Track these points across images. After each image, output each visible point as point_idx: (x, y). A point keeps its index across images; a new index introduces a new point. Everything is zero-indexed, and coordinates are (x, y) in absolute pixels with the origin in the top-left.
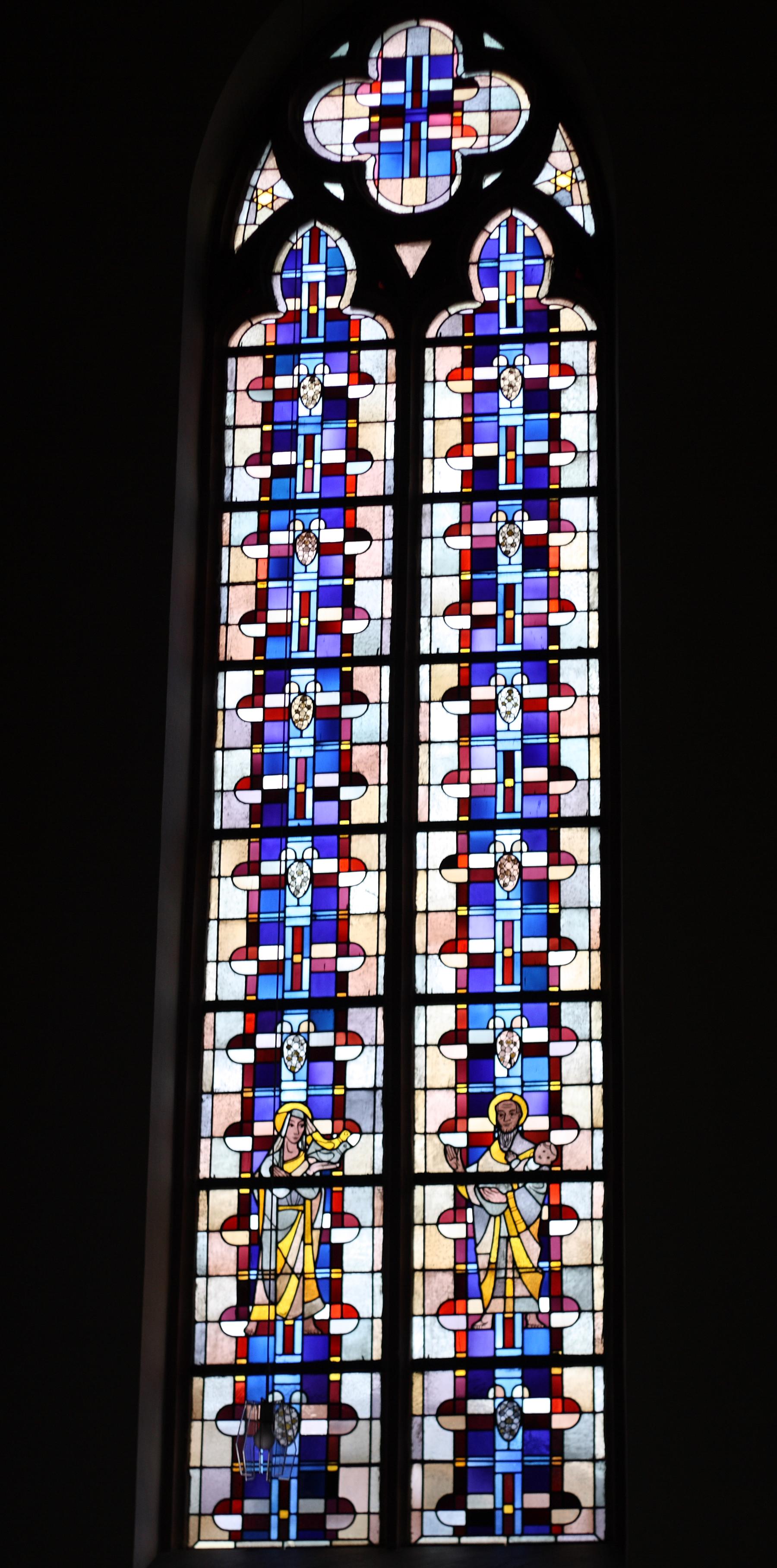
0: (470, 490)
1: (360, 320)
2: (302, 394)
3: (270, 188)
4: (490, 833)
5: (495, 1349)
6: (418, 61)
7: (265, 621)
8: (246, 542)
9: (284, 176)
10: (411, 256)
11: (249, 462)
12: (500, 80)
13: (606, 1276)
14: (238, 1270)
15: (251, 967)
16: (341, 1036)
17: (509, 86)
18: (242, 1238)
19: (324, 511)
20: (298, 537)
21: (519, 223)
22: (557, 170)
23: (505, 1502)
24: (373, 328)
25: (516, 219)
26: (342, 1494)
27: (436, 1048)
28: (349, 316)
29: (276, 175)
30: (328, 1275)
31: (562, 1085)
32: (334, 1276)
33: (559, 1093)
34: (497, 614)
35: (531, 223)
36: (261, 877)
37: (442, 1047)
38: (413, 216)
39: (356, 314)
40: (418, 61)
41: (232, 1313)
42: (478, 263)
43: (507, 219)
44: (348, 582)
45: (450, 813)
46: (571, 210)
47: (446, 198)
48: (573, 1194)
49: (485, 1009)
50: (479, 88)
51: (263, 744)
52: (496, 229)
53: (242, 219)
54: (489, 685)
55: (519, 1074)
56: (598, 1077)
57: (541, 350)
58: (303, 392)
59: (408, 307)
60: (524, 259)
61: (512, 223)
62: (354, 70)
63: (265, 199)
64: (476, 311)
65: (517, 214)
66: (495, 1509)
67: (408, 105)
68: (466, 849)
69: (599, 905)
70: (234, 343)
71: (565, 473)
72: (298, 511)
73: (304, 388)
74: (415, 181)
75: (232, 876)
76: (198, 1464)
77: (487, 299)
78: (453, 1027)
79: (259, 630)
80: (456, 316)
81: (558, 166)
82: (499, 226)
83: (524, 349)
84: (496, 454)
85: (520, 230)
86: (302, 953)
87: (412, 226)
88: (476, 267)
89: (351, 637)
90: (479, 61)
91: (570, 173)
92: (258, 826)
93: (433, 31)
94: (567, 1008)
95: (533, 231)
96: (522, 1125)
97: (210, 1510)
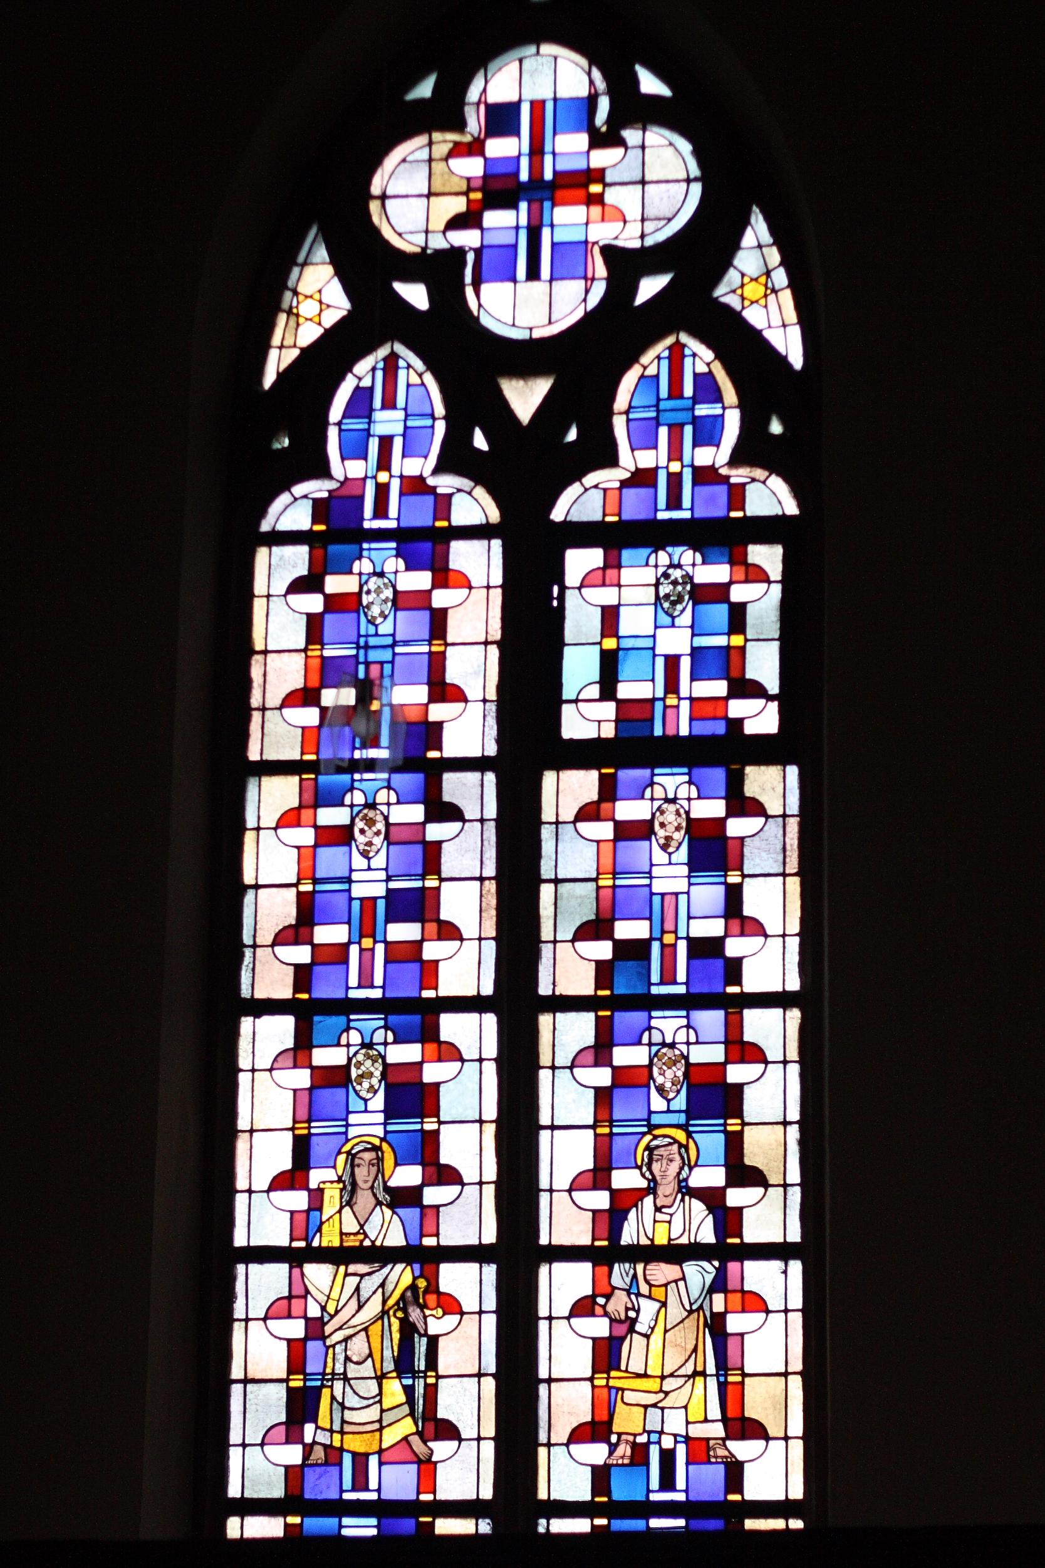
0: (605, 1243)
1: (451, 495)
2: (365, 603)
3: (319, 295)
4: (647, 772)
5: (656, 510)
6: (533, 273)
7: (309, 941)
8: (280, 939)
9: (339, 273)
10: (525, 398)
11: (278, 941)
12: (656, 136)
13: (803, 1076)
14: (295, 1122)
15: (306, 836)
16: (431, 1047)
17: (671, 144)
18: (298, 1200)
19: (391, 1018)
20: (357, 814)
21: (687, 352)
22: (743, 275)
23: (667, 691)
24: (473, 506)
25: (684, 346)
26: (444, 1160)
27: (577, 591)
28: (435, 488)
29: (329, 270)
30: (418, 1127)
31: (744, 1124)
32: (427, 1127)
33: (741, 1134)
34: (651, 939)
35: (708, 355)
36: (315, 947)
37: (577, 944)
38: (531, 343)
39: (445, 483)
40: (533, 273)
41: (590, 1057)
42: (627, 413)
43: (670, 348)
44: (431, 883)
45: (583, 984)
46: (767, 334)
47: (579, 314)
48: (760, 1025)
49: (636, 1018)
50: (626, 149)
51: (322, 644)
52: (653, 359)
53: (276, 340)
54: (642, 798)
55: (690, 624)
56: (794, 1114)
57: (711, 1020)
58: (365, 600)
59: (524, 471)
60: (389, 879)
61: (677, 354)
62: (445, 113)
63: (307, 308)
64: (624, 484)
65: (684, 338)
66: (657, 468)
67: (524, 176)
68: (609, 791)
69: (798, 1181)
70: (265, 527)
71: (748, 1093)
72: (352, 1017)
73: (368, 592)
74: (538, 96)
75: (273, 945)
76: (242, 1376)
77: (640, 466)
78: (593, 917)
79: (302, 954)
80: (593, 490)
81: (745, 271)
82: (659, 358)
83: (687, 1017)
84: (647, 936)
85: (688, 362)
86: (373, 936)
87: (526, 357)
88: (624, 417)
89: (444, 612)
90: (633, 110)
91: (763, 280)
92: (322, 527)
93: (559, 60)
94: (751, 1016)
95: (708, 364)
96: (686, 1180)
97: (277, 702)
